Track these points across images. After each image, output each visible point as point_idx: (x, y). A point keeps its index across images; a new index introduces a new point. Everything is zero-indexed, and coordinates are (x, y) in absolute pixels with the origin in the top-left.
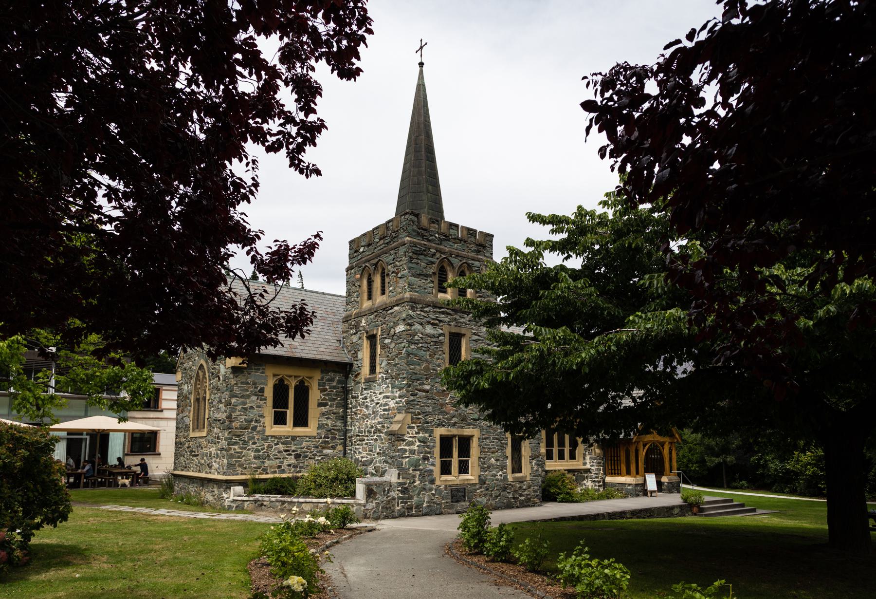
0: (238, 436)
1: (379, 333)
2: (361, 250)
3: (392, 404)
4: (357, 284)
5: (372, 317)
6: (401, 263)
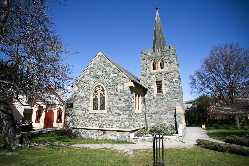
1: (164, 80)
2: (149, 54)
5: (159, 75)
6: (173, 60)
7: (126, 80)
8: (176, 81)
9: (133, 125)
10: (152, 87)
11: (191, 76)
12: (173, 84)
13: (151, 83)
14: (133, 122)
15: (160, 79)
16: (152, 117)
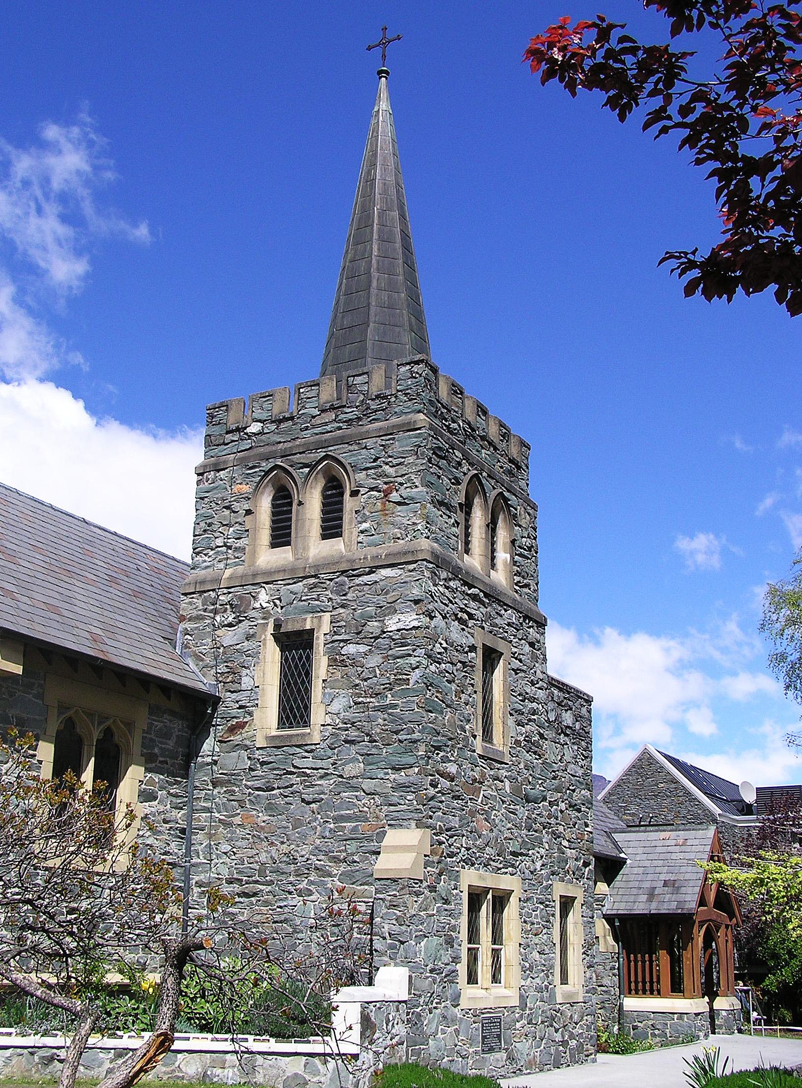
1: (326, 627)
2: (255, 428)
4: (241, 507)
5: (299, 587)
6: (403, 470)
8: (402, 638)
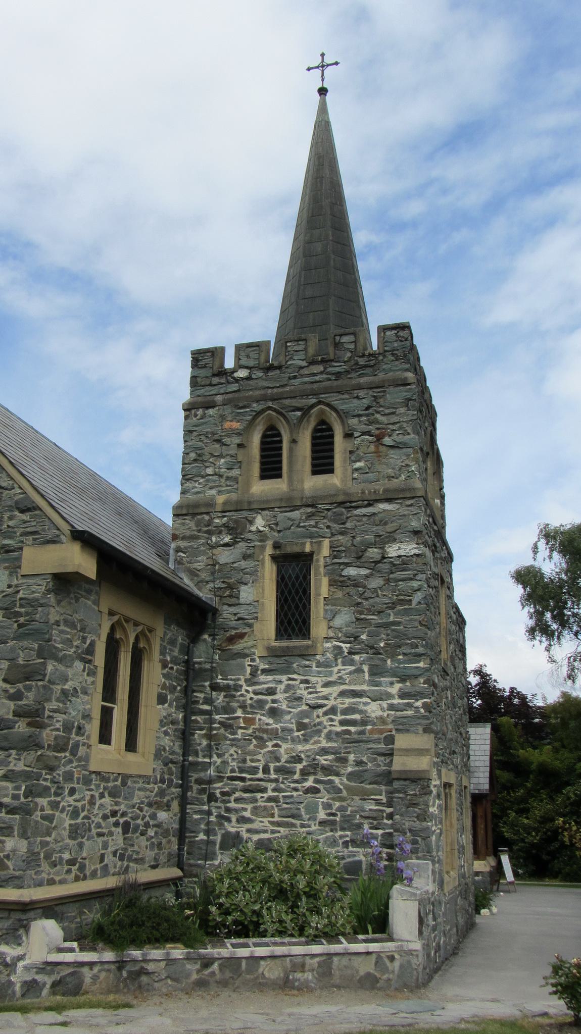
0: (51, 769)
1: (326, 551)
3: (374, 709)
5: (296, 514)
6: (394, 419)
7: (39, 528)
8: (404, 562)
9: (66, 856)
10: (246, 594)
11: (550, 994)
12: (388, 581)
13: (243, 564)
14: (65, 834)
15: (304, 544)
16: (232, 805)
